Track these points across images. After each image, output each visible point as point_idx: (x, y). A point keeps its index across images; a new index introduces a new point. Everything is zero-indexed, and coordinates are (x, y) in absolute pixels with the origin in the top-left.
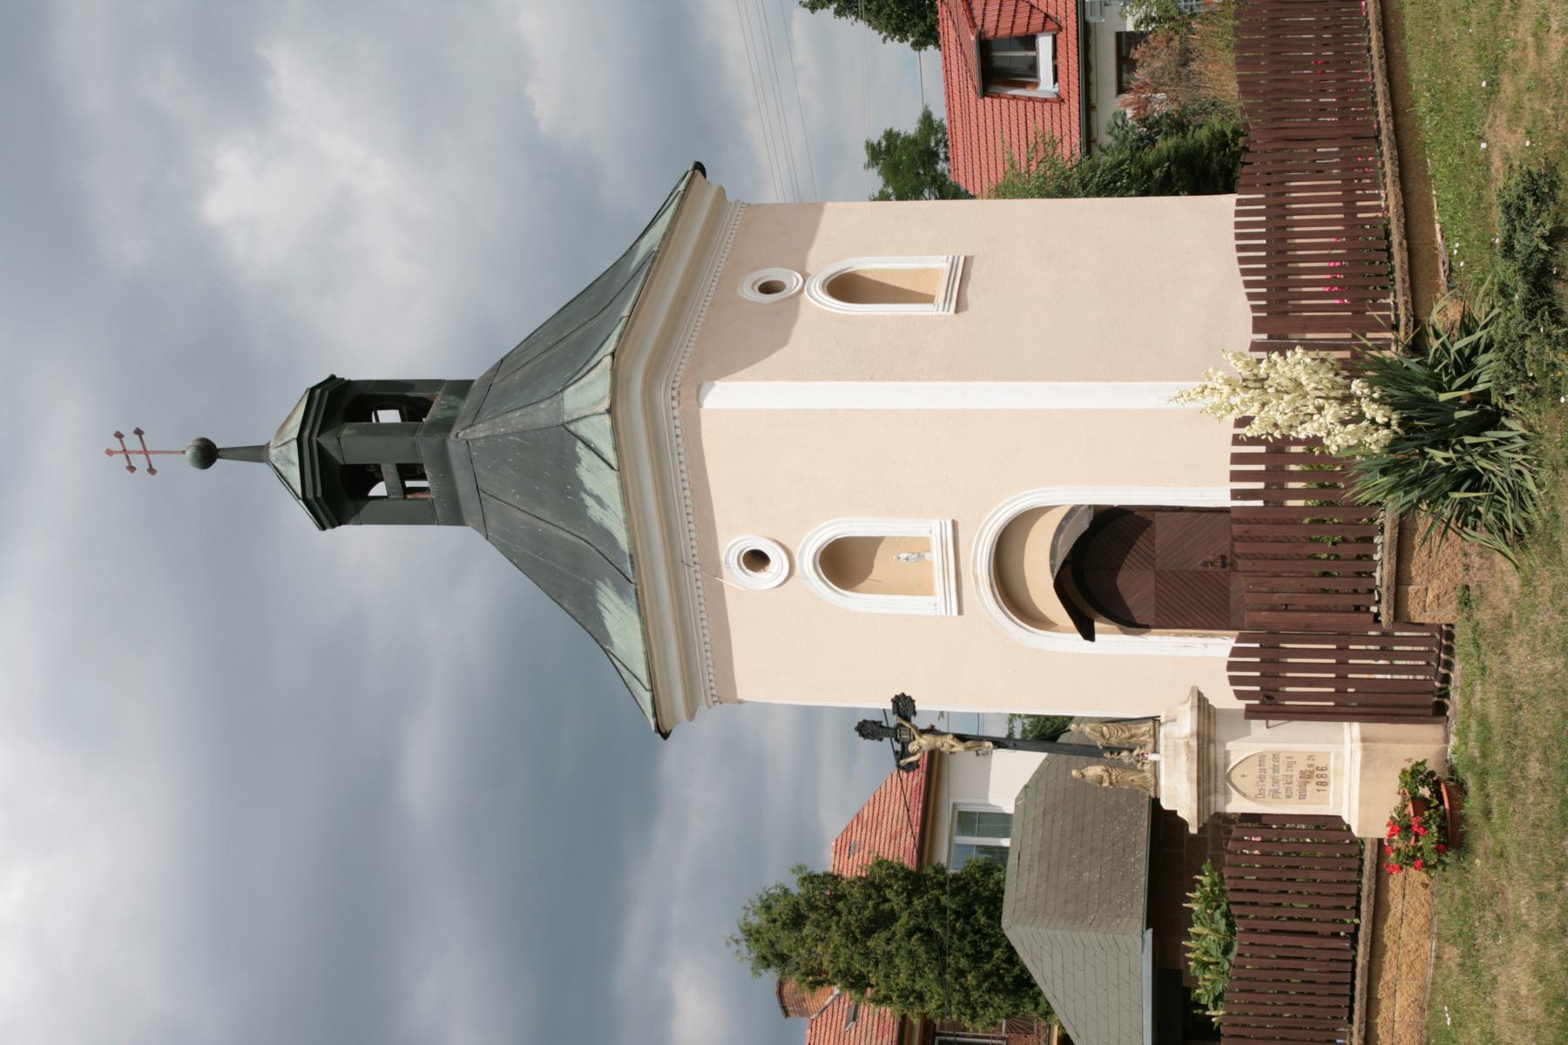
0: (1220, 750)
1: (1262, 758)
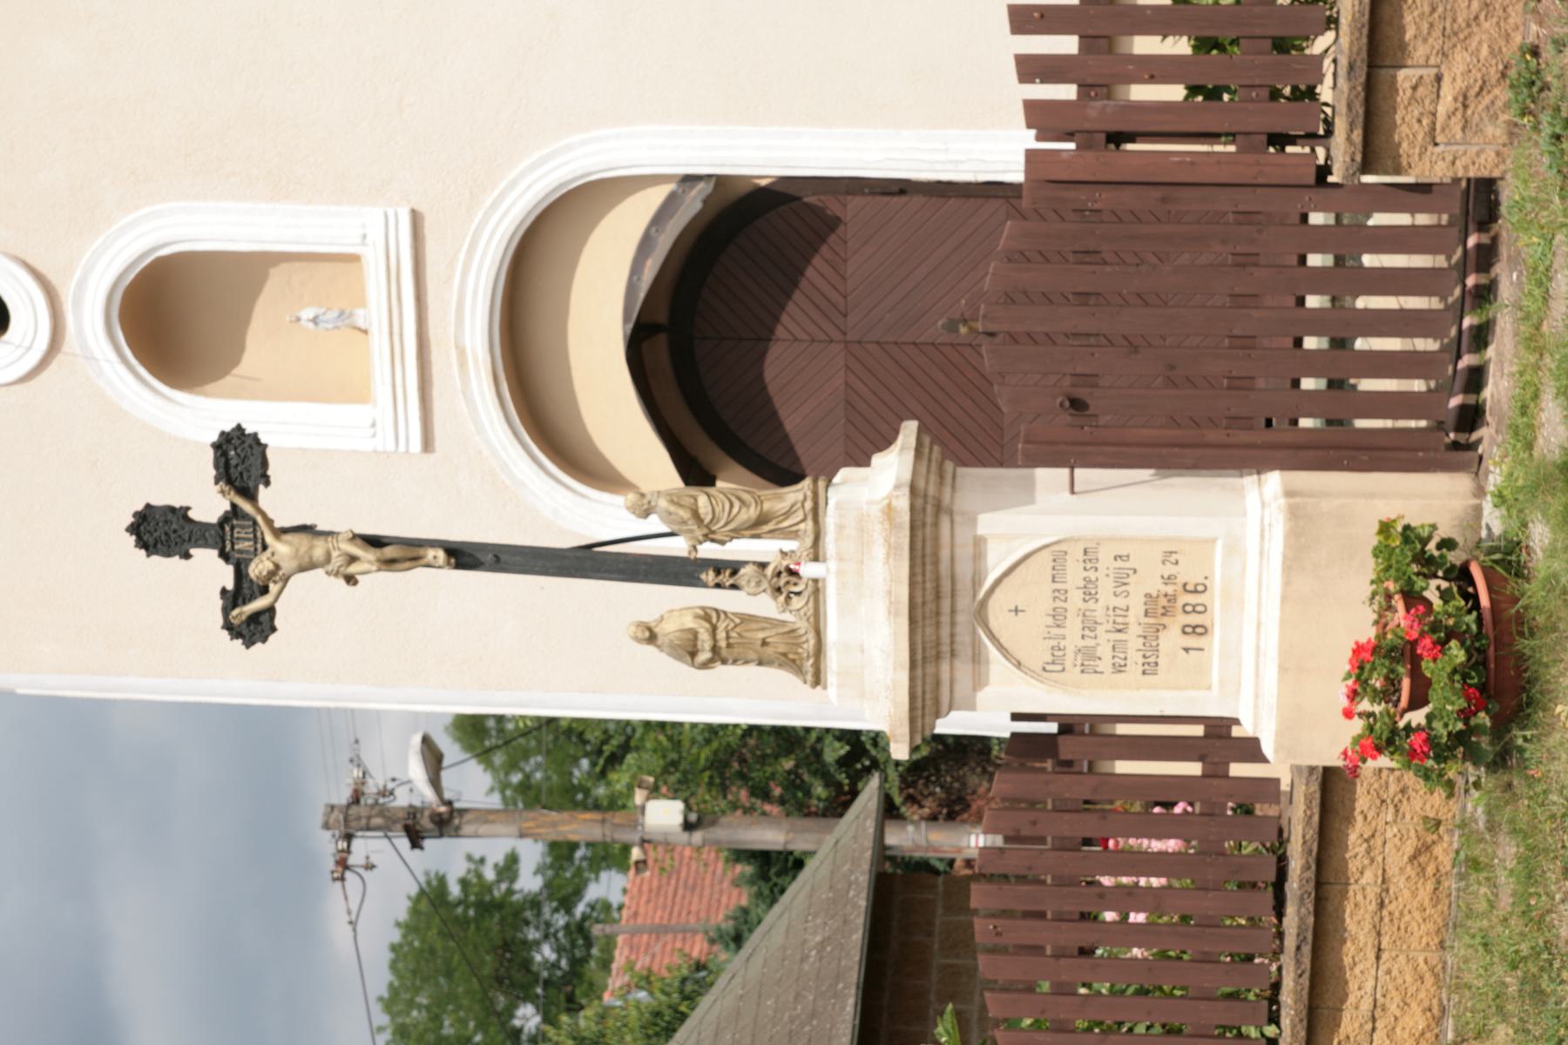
0: (963, 536)
1: (1056, 553)
